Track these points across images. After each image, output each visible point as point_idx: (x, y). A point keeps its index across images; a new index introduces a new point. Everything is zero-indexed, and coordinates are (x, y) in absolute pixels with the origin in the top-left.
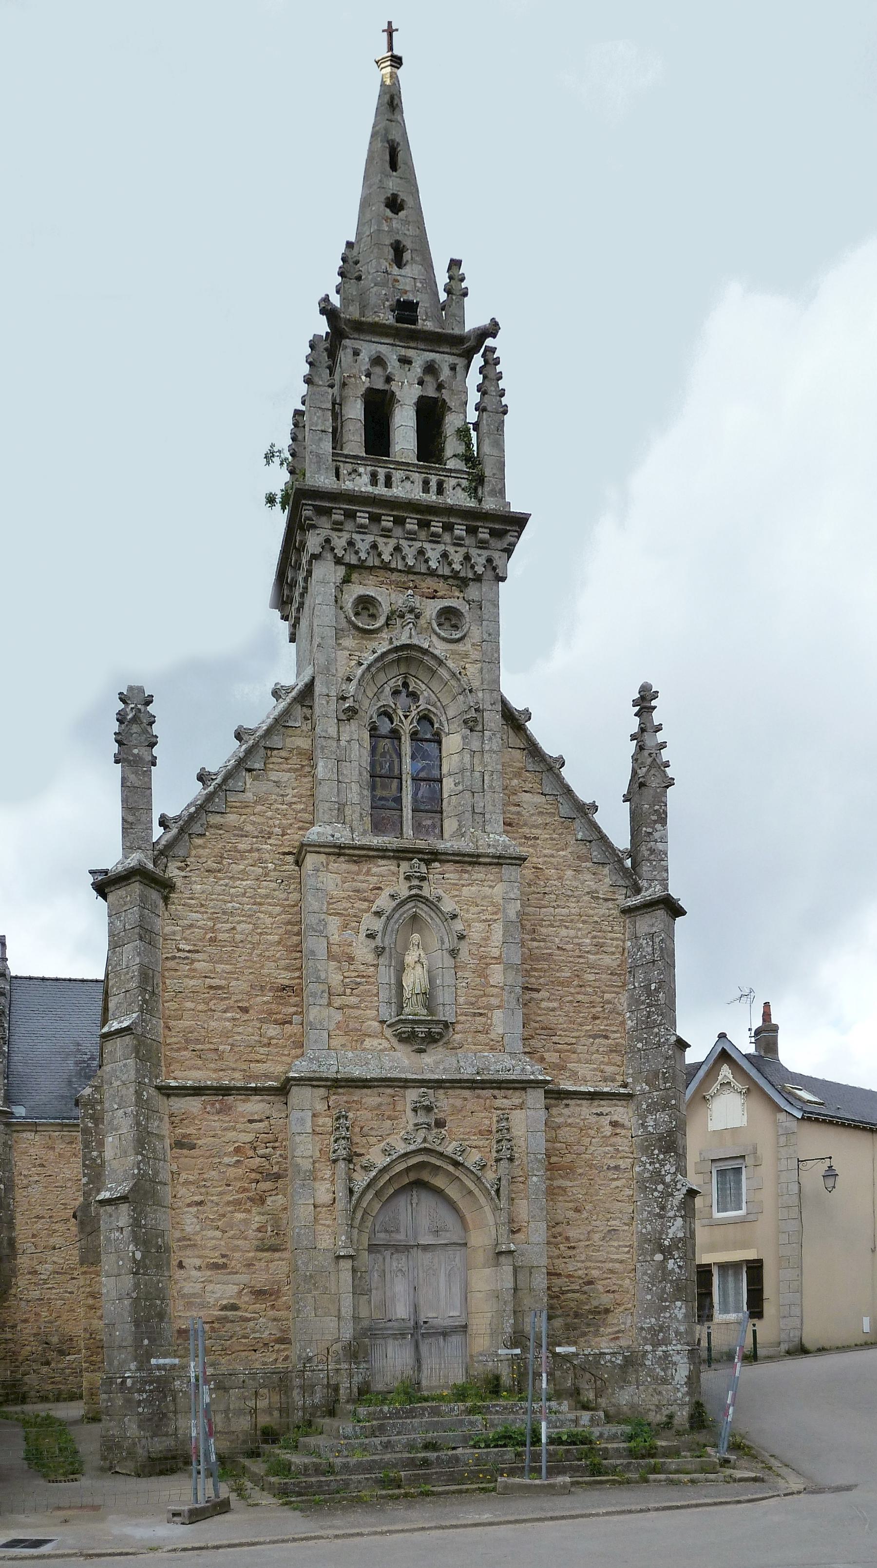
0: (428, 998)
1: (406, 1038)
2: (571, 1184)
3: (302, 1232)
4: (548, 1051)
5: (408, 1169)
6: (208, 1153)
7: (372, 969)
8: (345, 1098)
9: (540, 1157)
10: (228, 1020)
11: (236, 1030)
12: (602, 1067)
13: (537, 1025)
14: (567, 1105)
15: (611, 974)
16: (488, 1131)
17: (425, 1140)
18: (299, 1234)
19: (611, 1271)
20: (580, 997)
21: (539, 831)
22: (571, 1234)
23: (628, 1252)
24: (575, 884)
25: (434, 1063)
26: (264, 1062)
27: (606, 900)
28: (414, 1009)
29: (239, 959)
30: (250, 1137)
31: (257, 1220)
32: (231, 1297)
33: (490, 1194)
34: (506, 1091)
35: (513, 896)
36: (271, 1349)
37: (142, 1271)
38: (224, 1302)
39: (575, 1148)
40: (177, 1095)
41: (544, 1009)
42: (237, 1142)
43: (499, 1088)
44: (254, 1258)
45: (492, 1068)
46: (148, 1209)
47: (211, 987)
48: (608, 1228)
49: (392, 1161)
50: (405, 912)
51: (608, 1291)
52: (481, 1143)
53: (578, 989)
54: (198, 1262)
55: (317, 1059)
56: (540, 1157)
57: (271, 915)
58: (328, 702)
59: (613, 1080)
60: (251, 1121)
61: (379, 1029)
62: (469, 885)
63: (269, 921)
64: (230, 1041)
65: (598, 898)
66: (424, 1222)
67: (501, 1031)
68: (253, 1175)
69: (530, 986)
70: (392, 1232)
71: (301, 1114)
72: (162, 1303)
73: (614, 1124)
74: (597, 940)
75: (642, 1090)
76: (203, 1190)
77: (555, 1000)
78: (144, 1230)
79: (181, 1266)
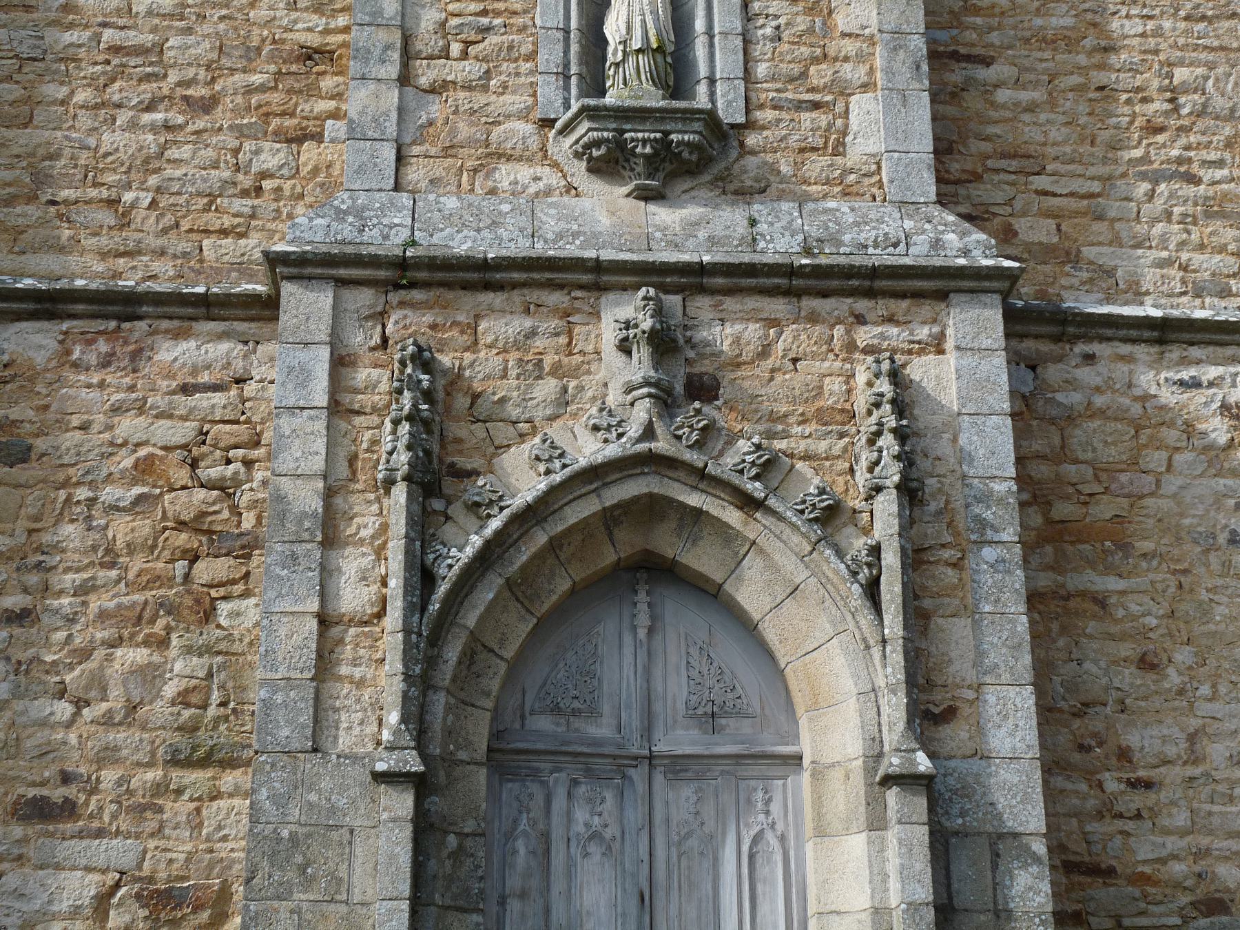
0: (672, 63)
1: (609, 162)
2: (1121, 585)
3: (279, 698)
4: (1024, 214)
5: (612, 518)
8: (428, 318)
10: (153, 128)
11: (173, 153)
13: (986, 147)
14: (1090, 358)
16: (843, 411)
17: (649, 433)
18: (267, 705)
22: (1133, 739)
25: (686, 227)
26: (243, 235)
28: (628, 87)
30: (182, 432)
31: (182, 668)
39: (1124, 478)
41: (1004, 106)
43: (871, 294)
44: (160, 789)
45: (847, 238)
47: (116, 49)
49: (552, 490)
52: (822, 446)
55: (358, 212)
60: (186, 389)
61: (534, 143)
64: (153, 181)
66: (675, 689)
69: (963, 51)
70: (575, 712)
71: (302, 355)
77: (1036, 84)
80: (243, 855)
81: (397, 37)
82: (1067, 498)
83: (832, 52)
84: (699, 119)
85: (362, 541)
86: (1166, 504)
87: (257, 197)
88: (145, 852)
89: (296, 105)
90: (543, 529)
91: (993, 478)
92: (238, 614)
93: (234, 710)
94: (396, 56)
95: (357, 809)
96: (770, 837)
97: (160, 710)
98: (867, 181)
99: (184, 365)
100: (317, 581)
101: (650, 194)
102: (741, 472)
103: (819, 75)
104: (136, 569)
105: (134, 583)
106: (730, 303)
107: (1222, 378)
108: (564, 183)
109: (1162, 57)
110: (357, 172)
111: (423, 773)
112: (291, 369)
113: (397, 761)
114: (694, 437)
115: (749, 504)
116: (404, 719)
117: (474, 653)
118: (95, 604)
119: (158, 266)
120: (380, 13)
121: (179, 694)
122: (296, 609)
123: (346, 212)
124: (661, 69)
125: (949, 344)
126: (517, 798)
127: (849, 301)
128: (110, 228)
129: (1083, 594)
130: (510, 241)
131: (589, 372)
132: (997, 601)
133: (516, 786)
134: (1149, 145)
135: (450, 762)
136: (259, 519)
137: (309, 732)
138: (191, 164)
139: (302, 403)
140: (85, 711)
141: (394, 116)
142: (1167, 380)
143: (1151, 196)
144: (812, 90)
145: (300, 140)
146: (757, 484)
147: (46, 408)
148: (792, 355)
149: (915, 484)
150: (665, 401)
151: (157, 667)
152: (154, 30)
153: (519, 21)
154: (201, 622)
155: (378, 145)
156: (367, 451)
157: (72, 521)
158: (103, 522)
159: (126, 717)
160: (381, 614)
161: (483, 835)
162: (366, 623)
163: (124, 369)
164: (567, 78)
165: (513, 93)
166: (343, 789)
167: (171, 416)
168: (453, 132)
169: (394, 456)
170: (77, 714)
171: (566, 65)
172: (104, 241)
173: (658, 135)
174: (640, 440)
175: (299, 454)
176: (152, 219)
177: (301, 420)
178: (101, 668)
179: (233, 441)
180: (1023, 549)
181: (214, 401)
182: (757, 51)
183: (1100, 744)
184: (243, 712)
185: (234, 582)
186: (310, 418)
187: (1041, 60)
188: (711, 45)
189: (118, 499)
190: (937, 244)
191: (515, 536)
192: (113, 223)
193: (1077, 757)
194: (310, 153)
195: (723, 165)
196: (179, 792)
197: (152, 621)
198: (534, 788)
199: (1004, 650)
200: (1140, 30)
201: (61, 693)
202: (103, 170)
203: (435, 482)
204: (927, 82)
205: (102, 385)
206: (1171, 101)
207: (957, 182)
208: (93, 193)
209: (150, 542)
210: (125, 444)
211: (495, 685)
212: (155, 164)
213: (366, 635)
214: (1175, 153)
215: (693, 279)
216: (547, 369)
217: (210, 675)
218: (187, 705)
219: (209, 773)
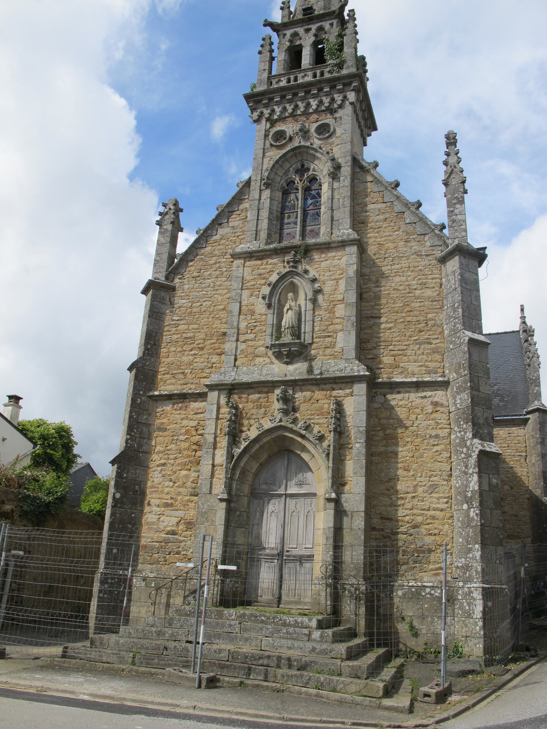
0: (296, 331)
1: (279, 356)
3: (203, 482)
4: (386, 356)
7: (264, 317)
9: (361, 429)
10: (192, 355)
11: (195, 360)
15: (431, 301)
17: (281, 421)
19: (434, 518)
20: (409, 319)
21: (381, 223)
23: (447, 503)
24: (405, 249)
25: (296, 370)
26: (208, 378)
27: (427, 256)
28: (287, 339)
29: (202, 321)
30: (194, 423)
31: (194, 475)
32: (173, 526)
34: (341, 385)
35: (352, 262)
37: (119, 505)
38: (169, 529)
40: (160, 400)
43: (336, 383)
44: (189, 501)
45: (331, 370)
46: (131, 468)
47: (185, 338)
48: (431, 483)
50: (285, 282)
51: (430, 534)
52: (321, 421)
54: (157, 502)
57: (221, 295)
58: (256, 183)
59: (436, 373)
60: (196, 414)
62: (326, 260)
63: (220, 298)
64: (191, 367)
65: (421, 255)
68: (194, 447)
69: (374, 315)
72: (133, 527)
73: (435, 404)
74: (421, 281)
75: (454, 377)
76: (166, 456)
78: (124, 480)
79: (149, 504)
81: (236, 330)
82: (390, 428)
83: (334, 323)
94: (236, 335)
96: (311, 511)
97: (189, 484)
103: (331, 328)
106: (304, 388)
107: (432, 395)
115: (303, 437)
116: (225, 487)
117: (244, 472)
120: (233, 325)
129: (392, 452)
130: (255, 377)
135: (238, 496)
138: (200, 363)
145: (220, 355)
150: (286, 412)
152: (193, 332)
153: (263, 323)
164: (272, 336)
171: (272, 333)
172: (181, 382)
174: (279, 422)
177: (210, 421)
178: (178, 475)
182: (315, 324)
188: (305, 324)
193: (386, 492)
195: (306, 353)
196: (192, 502)
198: (261, 501)
201: (171, 481)
203: (234, 436)
206: (426, 323)
207: (369, 350)
212: (192, 363)
214: (426, 337)
215: (295, 384)
217: (198, 477)
218: (194, 483)
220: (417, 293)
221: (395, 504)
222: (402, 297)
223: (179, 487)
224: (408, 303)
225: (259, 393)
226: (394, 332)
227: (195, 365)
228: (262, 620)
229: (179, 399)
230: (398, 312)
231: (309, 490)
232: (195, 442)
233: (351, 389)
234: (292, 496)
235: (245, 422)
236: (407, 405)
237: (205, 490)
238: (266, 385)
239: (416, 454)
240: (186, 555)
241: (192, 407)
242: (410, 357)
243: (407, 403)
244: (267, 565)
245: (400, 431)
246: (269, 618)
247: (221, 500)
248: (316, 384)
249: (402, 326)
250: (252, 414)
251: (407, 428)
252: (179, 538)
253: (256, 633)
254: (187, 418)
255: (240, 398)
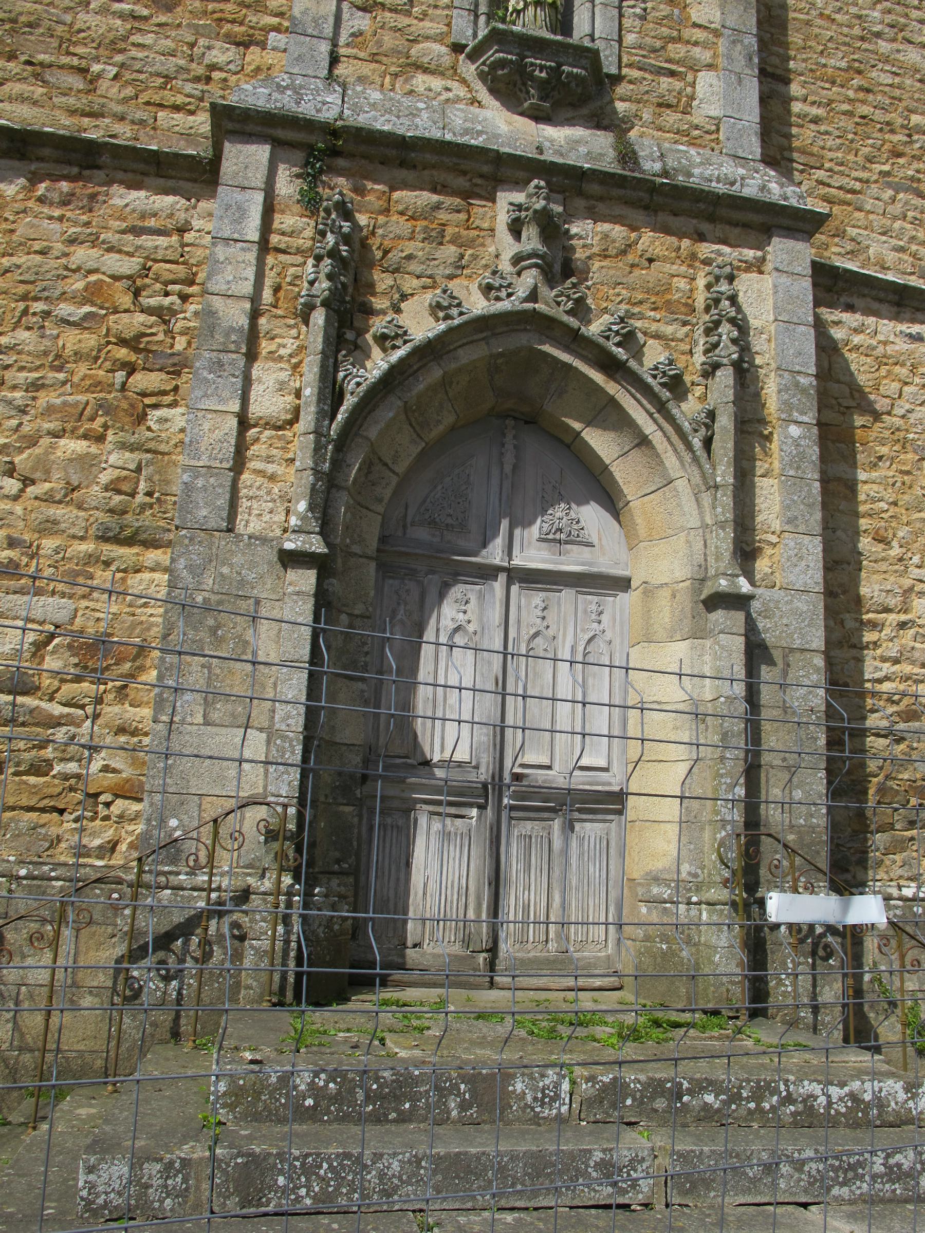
3: (200, 483)
6: (22, 289)
10: (121, 16)
11: (137, 38)
12: (914, 248)
16: (686, 305)
17: (533, 296)
20: (865, 110)
25: (568, 142)
26: (192, 113)
30: (128, 266)
31: (116, 460)
33: (689, 446)
36: (102, 811)
42: (96, 271)
44: (91, 559)
45: (696, 171)
52: (669, 330)
53: (861, 95)
56: (802, 380)
60: (137, 231)
67: (715, 111)
80: (160, 620)
84: (586, 57)
85: (281, 357)
86: (898, 422)
87: (207, 84)
88: (76, 610)
89: (245, 16)
90: (439, 365)
91: (799, 372)
92: (166, 420)
93: (158, 499)
95: (264, 584)
98: (708, 137)
99: (134, 211)
100: (239, 386)
101: (541, 114)
102: (608, 338)
103: (677, 50)
104: (81, 374)
105: (79, 385)
106: (601, 207)
108: (469, 96)
109: (904, 104)
110: (297, 59)
111: (325, 555)
112: (228, 207)
113: (304, 542)
114: (570, 305)
116: (311, 508)
117: (371, 464)
118: (44, 399)
119: (118, 128)
121: (112, 482)
122: (220, 408)
123: (287, 88)
124: (554, 22)
125: (769, 266)
126: (397, 592)
127: (695, 221)
128: (79, 91)
129: (839, 479)
131: (483, 245)
132: (798, 468)
133: (397, 582)
134: (893, 164)
136: (189, 343)
137: (225, 514)
139: (236, 236)
140: (29, 490)
141: (331, 20)
142: (901, 332)
143: (893, 200)
144: (669, 61)
146: (620, 350)
147: (12, 231)
148: (648, 255)
149: (746, 365)
151: (96, 457)
154: (133, 424)
155: (315, 40)
156: (290, 284)
157: (29, 329)
158: (55, 332)
159: (66, 496)
160: (295, 419)
161: (368, 617)
162: (280, 428)
163: (82, 208)
164: (477, 17)
165: (431, 21)
166: (252, 565)
167: (120, 252)
168: (379, 44)
169: (316, 284)
170: (22, 491)
173: (553, 64)
174: (526, 300)
175: (231, 278)
176: (115, 90)
179: (172, 277)
180: (820, 430)
181: (157, 243)
183: (844, 593)
184: (165, 502)
185: (164, 393)
186: (243, 249)
187: (823, 88)
189: (69, 315)
190: (763, 188)
191: (415, 367)
192: (81, 87)
194: (254, 55)
195: (599, 103)
196: (107, 564)
197: (92, 419)
199: (802, 507)
200: (890, 82)
202: (75, 44)
203: (347, 316)
204: (757, 71)
205: (61, 219)
208: (65, 60)
209: (94, 353)
210: (78, 269)
211: (388, 493)
213: (279, 438)
214: (910, 173)
216: (447, 238)
217: (139, 470)
218: (119, 492)
219: (135, 550)
220: (884, 46)
221: (854, 640)
222: (845, 44)
223: (48, 499)
224: (862, 67)
225: (434, 190)
226: (827, 133)
227: (134, 52)
228: (706, 1106)
229: (57, 161)
230: (833, 83)
231: (590, 564)
232: (127, 335)
233: (758, 249)
234: (532, 578)
235: (383, 281)
236: (874, 348)
237: (207, 511)
238: (466, 165)
239: (906, 497)
240: (78, 776)
241: (117, 202)
242: (871, 217)
243: (874, 342)
244: (437, 826)
245: (859, 421)
246: (735, 1098)
247: (289, 559)
248: (646, 208)
249: (847, 124)
250: (409, 257)
251: (877, 416)
252: (44, 705)
253: (747, 1191)
254: (94, 242)
255: (360, 190)
